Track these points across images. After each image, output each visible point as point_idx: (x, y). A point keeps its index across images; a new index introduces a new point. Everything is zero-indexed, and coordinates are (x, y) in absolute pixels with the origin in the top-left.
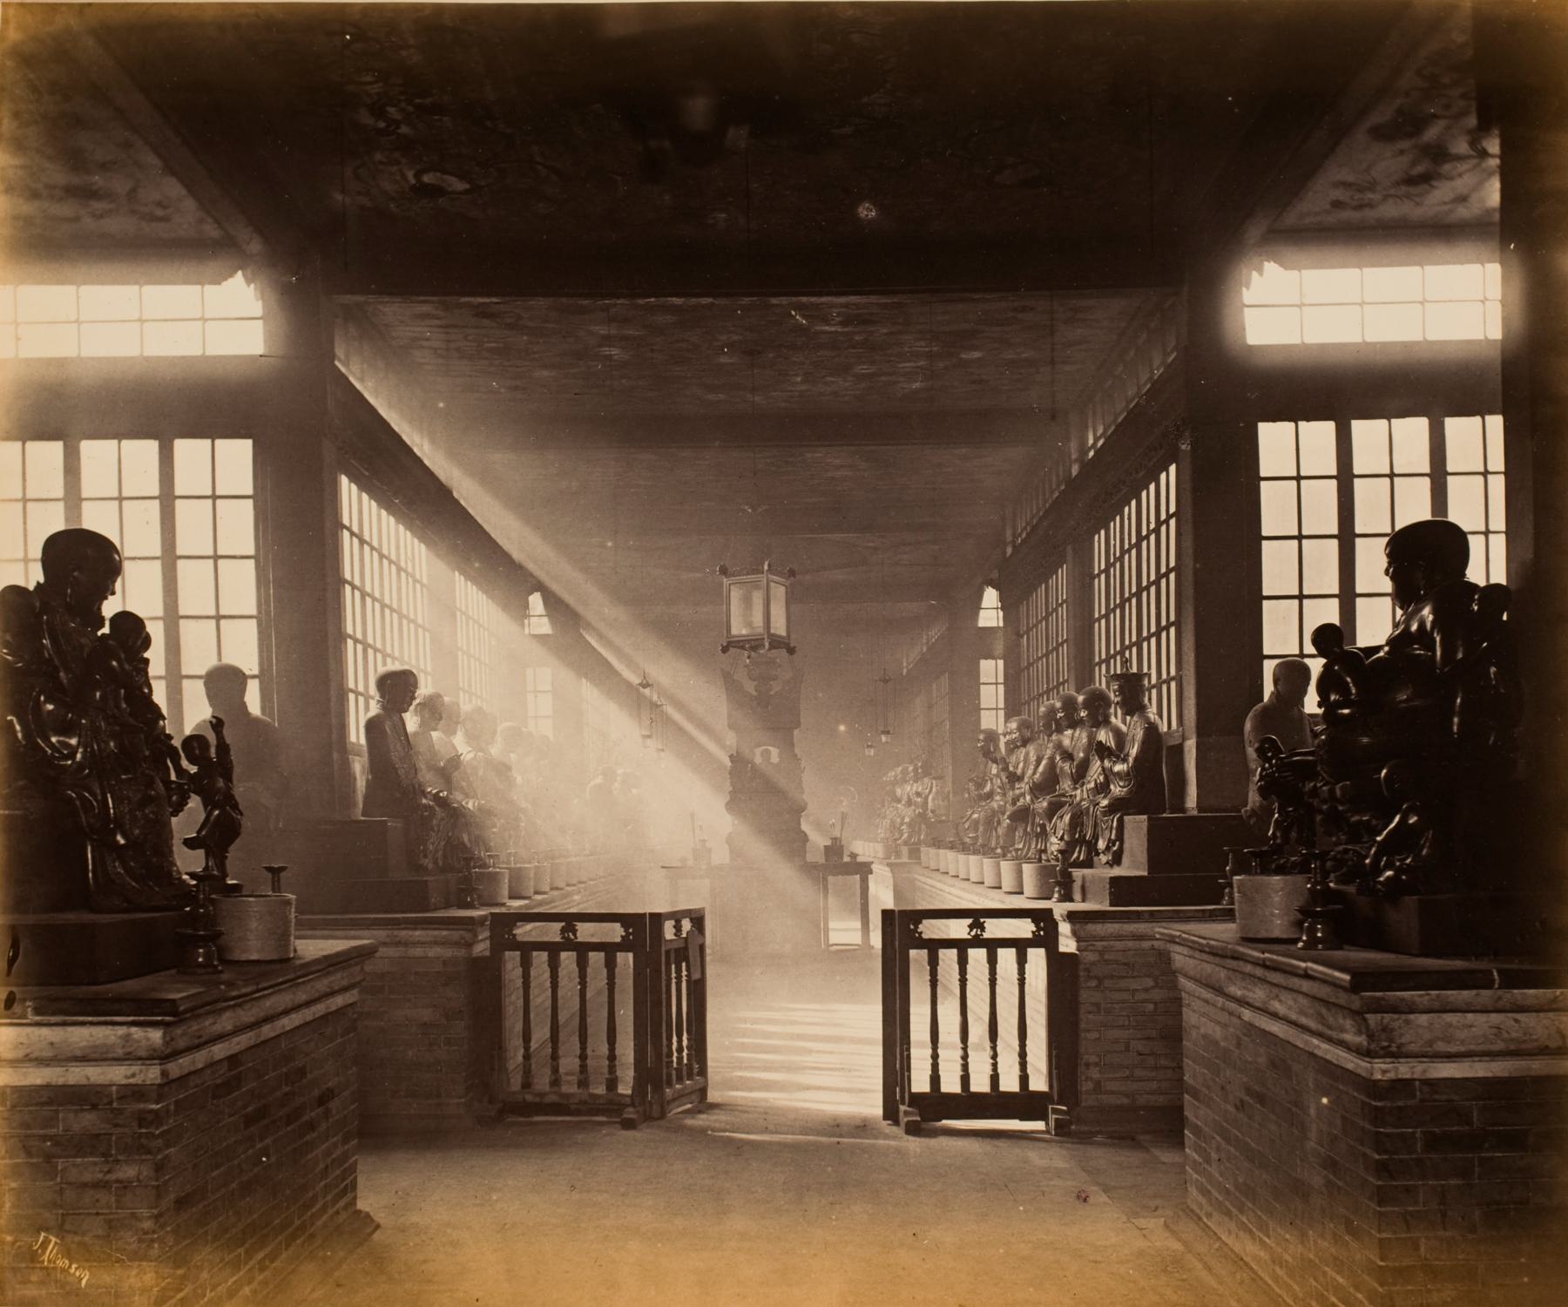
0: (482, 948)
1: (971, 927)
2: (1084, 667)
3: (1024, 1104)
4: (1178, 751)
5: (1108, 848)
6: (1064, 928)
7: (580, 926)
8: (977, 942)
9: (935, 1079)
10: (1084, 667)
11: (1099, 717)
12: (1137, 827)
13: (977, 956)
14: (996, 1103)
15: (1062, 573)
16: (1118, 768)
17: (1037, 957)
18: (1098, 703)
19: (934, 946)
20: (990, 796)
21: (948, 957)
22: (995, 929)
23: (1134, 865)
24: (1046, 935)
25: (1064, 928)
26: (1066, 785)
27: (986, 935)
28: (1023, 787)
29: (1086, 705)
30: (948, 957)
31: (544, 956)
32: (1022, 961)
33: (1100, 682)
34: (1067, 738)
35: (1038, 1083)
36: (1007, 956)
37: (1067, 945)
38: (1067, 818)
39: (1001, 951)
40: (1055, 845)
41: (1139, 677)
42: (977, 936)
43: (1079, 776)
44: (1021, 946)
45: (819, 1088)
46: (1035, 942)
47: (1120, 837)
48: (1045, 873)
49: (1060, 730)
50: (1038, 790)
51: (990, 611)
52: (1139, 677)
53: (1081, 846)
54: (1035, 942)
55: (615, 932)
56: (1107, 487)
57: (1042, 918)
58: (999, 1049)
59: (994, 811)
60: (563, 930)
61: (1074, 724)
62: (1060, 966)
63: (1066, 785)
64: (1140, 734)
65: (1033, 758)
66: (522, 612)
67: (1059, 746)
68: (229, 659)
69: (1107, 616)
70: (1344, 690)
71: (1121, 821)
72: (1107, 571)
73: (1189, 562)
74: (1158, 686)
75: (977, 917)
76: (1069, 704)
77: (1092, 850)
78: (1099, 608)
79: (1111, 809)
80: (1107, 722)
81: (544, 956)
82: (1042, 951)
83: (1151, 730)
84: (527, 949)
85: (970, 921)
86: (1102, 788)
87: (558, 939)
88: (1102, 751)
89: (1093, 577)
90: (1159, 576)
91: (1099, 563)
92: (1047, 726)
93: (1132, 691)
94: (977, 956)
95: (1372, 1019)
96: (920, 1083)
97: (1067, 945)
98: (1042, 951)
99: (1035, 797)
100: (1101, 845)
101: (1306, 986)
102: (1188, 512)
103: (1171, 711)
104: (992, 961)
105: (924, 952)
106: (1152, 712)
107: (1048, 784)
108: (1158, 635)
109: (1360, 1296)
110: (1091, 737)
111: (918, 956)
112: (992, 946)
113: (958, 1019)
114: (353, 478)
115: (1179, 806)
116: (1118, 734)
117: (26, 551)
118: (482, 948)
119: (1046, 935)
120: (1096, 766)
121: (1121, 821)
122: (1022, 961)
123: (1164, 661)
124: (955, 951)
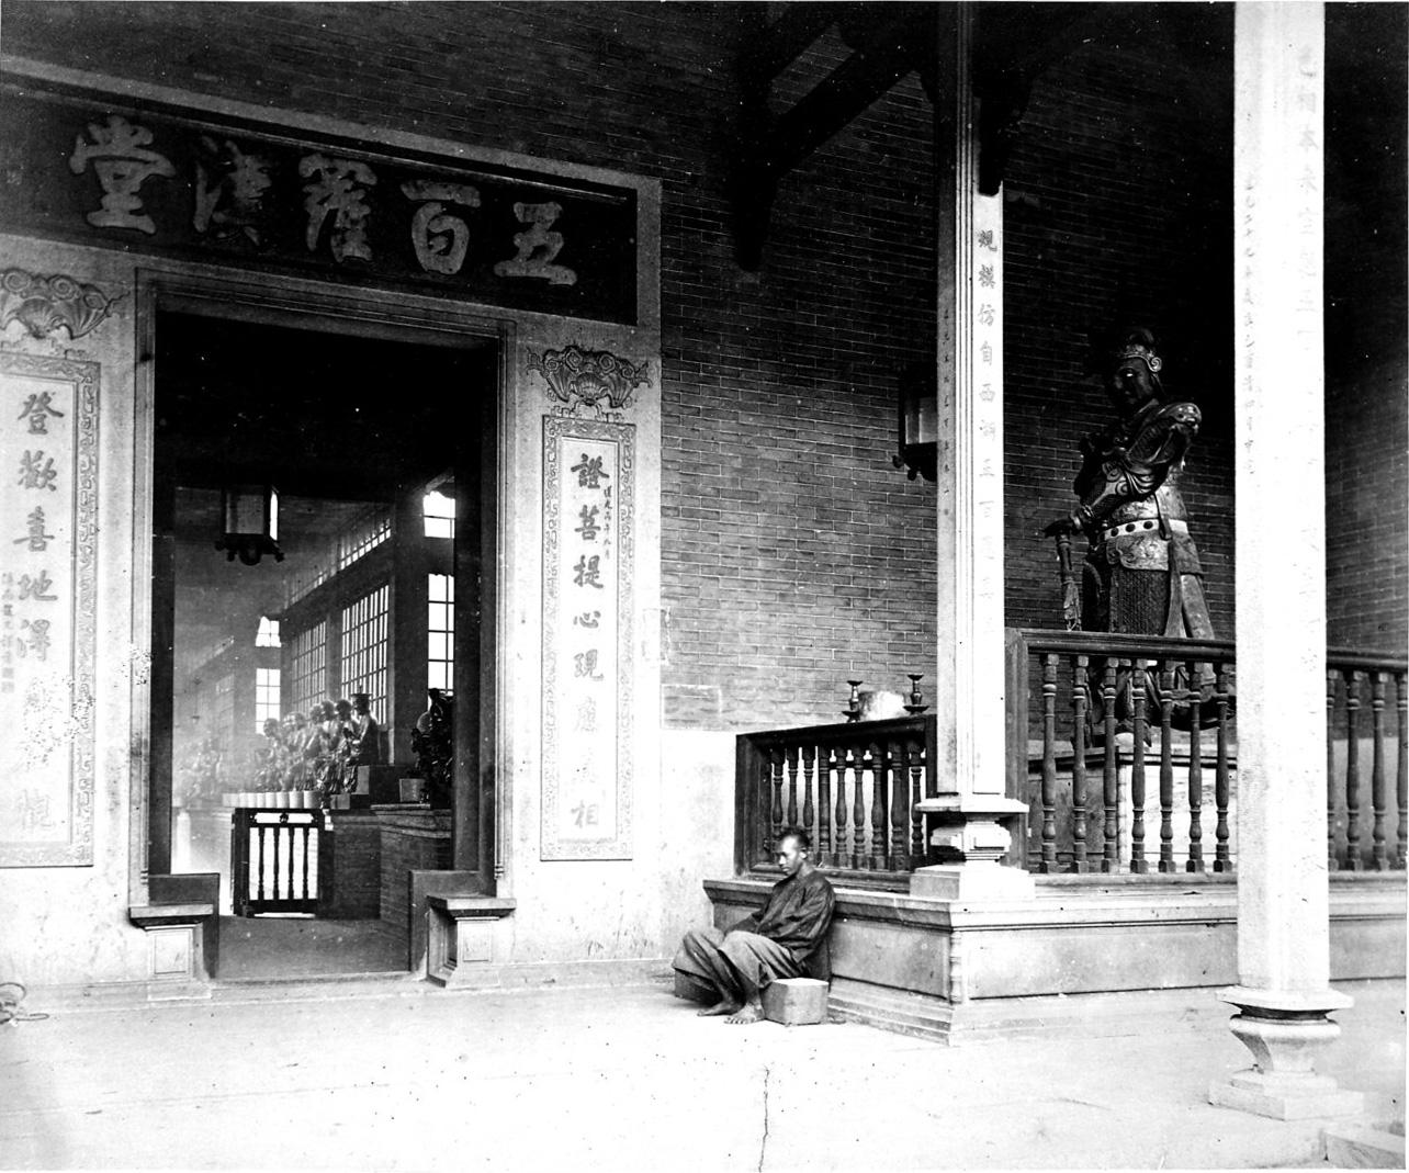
2: (335, 685)
3: (304, 905)
4: (386, 734)
6: (328, 819)
8: (284, 824)
10: (335, 685)
11: (345, 716)
12: (364, 772)
13: (284, 832)
14: (291, 904)
15: (323, 626)
16: (356, 742)
17: (314, 832)
18: (344, 706)
19: (262, 827)
20: (274, 760)
22: (293, 818)
23: (363, 788)
24: (318, 823)
25: (328, 819)
26: (326, 751)
28: (300, 753)
29: (338, 708)
33: (345, 697)
34: (326, 726)
36: (299, 832)
37: (329, 827)
38: (327, 769)
41: (367, 695)
43: (333, 747)
44: (306, 827)
46: (312, 825)
47: (356, 777)
49: (322, 721)
52: (367, 695)
53: (334, 781)
54: (312, 825)
56: (353, 585)
59: (277, 770)
61: (330, 717)
62: (323, 834)
63: (326, 751)
64: (366, 725)
65: (304, 736)
67: (321, 730)
68: (271, 716)
69: (349, 657)
70: (439, 712)
71: (356, 771)
72: (350, 632)
73: (393, 636)
74: (377, 700)
75: (285, 812)
76: (328, 707)
78: (345, 651)
79: (352, 763)
80: (349, 718)
83: (372, 723)
86: (346, 753)
88: (347, 733)
89: (342, 634)
90: (379, 615)
91: (346, 627)
92: (314, 718)
93: (363, 702)
94: (284, 832)
95: (438, 819)
96: (254, 896)
99: (306, 758)
100: (346, 781)
101: (420, 813)
102: (392, 641)
104: (292, 834)
106: (373, 715)
108: (378, 617)
109: (178, 119)
110: (341, 726)
111: (254, 832)
112: (292, 827)
113: (280, 849)
115: (387, 760)
116: (354, 724)
119: (318, 823)
120: (343, 741)
121: (356, 771)
122: (306, 834)
123: (380, 687)
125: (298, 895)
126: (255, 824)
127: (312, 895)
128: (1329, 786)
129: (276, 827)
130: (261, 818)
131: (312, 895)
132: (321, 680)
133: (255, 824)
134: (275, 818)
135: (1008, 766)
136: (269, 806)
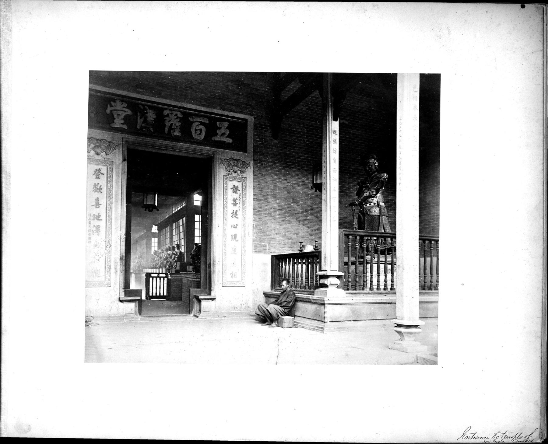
2: (171, 242)
3: (163, 297)
8: (158, 277)
10: (171, 242)
11: (174, 250)
12: (178, 264)
13: (158, 279)
14: (160, 297)
15: (168, 227)
17: (166, 279)
18: (173, 248)
19: (153, 277)
21: (155, 279)
22: (161, 275)
23: (178, 268)
33: (174, 245)
34: (169, 252)
35: (165, 294)
37: (170, 278)
40: (167, 267)
43: (171, 258)
44: (164, 278)
48: (166, 270)
50: (165, 259)
51: (155, 229)
56: (176, 217)
57: (166, 274)
61: (170, 250)
62: (168, 279)
75: (159, 274)
77: (172, 267)
83: (180, 252)
86: (174, 259)
88: (174, 254)
91: (174, 228)
93: (178, 247)
96: (151, 295)
97: (170, 278)
103: (183, 249)
107: (167, 258)
111: (151, 279)
112: (160, 278)
117: (330, 304)
123: (182, 243)
126: (151, 277)
127: (165, 294)
129: (156, 277)
130: (152, 275)
132: (168, 241)
133: (151, 277)
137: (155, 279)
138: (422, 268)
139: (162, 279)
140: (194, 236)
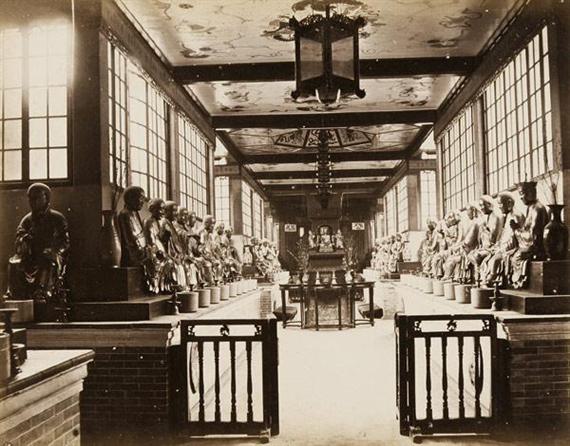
0: (176, 340)
1: (449, 325)
5: (520, 280)
7: (230, 327)
8: (225, 338)
9: (429, 411)
13: (224, 346)
17: (485, 341)
19: (428, 336)
21: (208, 346)
22: (462, 326)
24: (490, 332)
27: (457, 330)
30: (208, 346)
31: (439, 339)
32: (249, 349)
37: (501, 334)
39: (465, 339)
42: (452, 330)
44: (476, 335)
45: (445, 404)
46: (484, 333)
54: (484, 333)
55: (251, 330)
58: (448, 394)
59: (211, 232)
60: (222, 330)
62: (497, 345)
66: (210, 146)
75: (451, 319)
79: (523, 257)
81: (439, 339)
82: (488, 338)
84: (201, 340)
85: (448, 322)
87: (219, 334)
93: (529, 191)
96: (194, 416)
97: (501, 334)
98: (488, 338)
104: (428, 345)
105: (228, 343)
111: (419, 343)
112: (233, 340)
114: (187, 83)
118: (176, 340)
124: (212, 343)
125: (470, 413)
126: (420, 334)
127: (485, 413)
128: (476, 350)
129: (444, 336)
130: (426, 327)
131: (485, 413)
132: (474, 176)
133: (420, 334)
134: (442, 326)
135: (438, 439)
136: (319, 318)
137: (436, 342)
138: (212, 199)
139: (241, 346)
140: (69, 148)
